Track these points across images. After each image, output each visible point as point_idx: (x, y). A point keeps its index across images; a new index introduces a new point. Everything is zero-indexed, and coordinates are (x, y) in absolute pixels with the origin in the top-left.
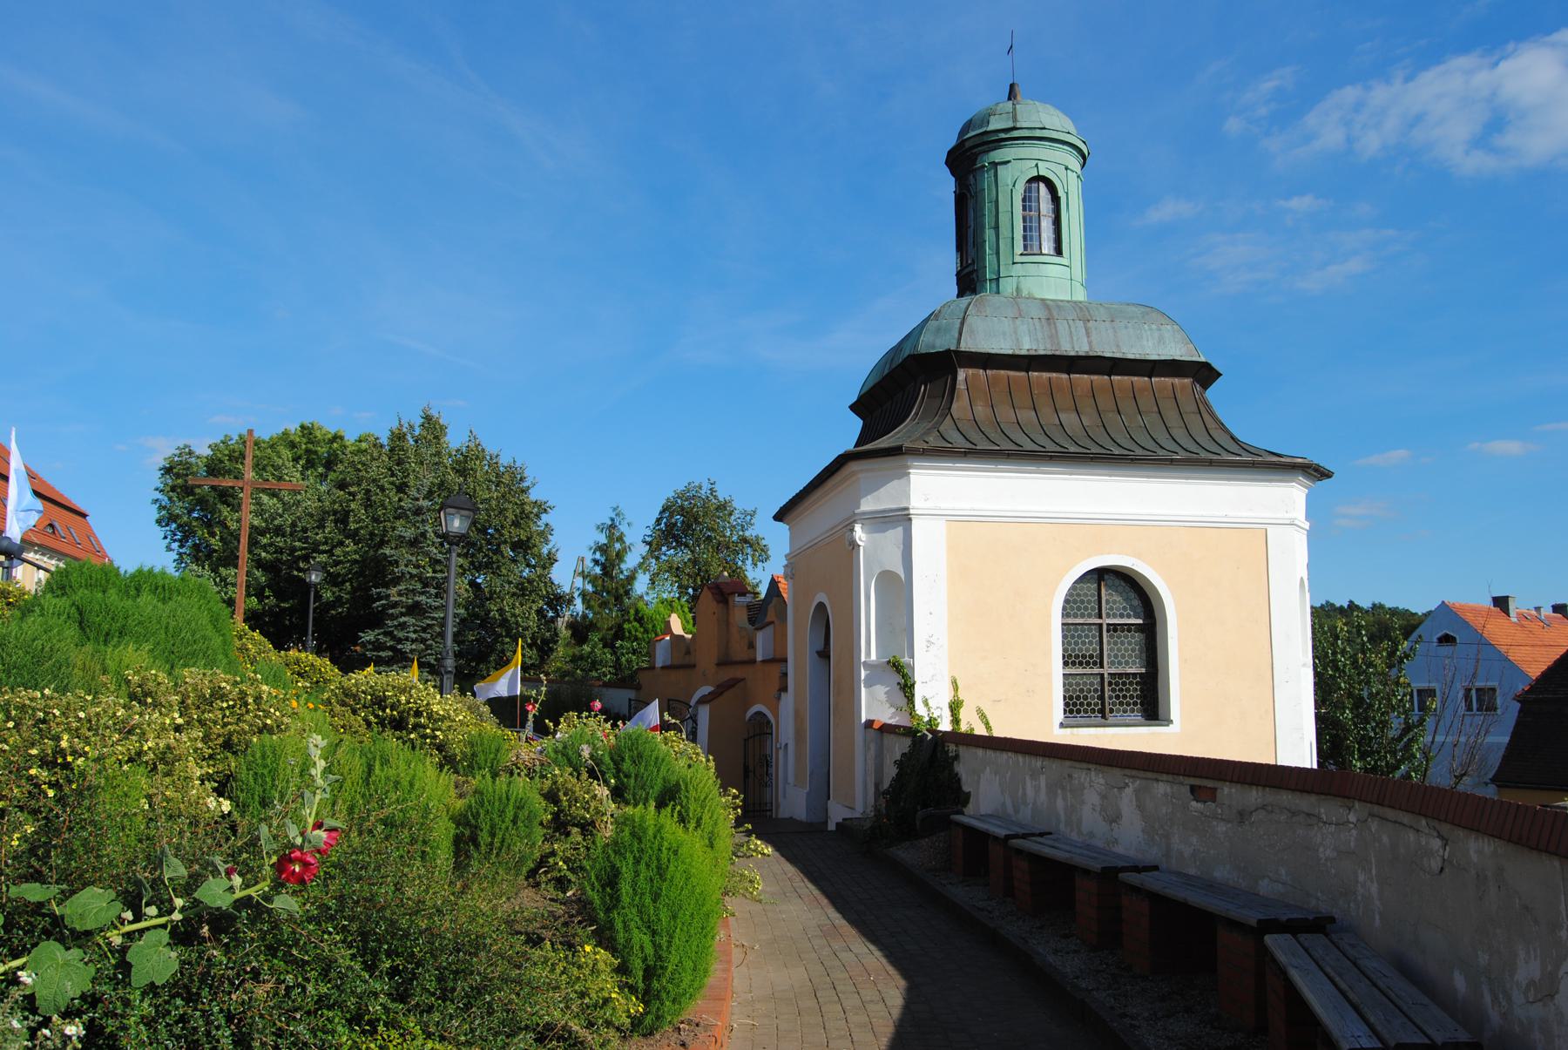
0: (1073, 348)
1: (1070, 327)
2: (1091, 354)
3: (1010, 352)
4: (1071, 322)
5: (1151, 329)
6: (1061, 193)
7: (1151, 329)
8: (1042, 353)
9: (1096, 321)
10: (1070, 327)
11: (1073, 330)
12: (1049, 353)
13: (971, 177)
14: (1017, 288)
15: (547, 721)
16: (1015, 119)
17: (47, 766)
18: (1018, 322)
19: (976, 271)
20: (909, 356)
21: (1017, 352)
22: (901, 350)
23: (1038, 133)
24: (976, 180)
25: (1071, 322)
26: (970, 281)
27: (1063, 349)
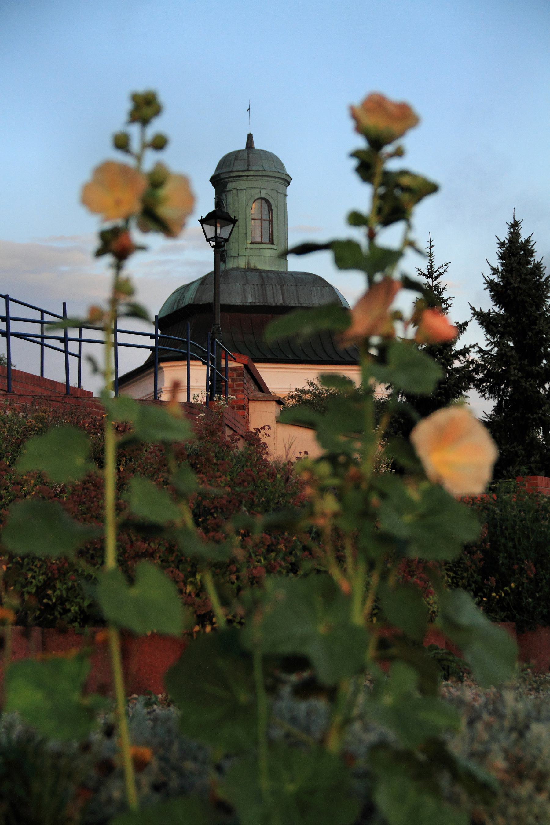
0: (274, 301)
1: (273, 289)
2: (284, 304)
3: (241, 304)
4: (274, 286)
5: (317, 290)
6: (273, 207)
7: (317, 290)
8: (258, 304)
9: (287, 285)
10: (273, 289)
11: (275, 291)
12: (261, 304)
13: (224, 195)
14: (248, 262)
15: (504, 407)
16: (248, 165)
17: (386, 448)
18: (246, 287)
19: (226, 251)
20: (189, 305)
21: (245, 304)
22: (184, 297)
23: (260, 173)
24: (226, 197)
25: (274, 286)
26: (260, 191)
27: (269, 302)
